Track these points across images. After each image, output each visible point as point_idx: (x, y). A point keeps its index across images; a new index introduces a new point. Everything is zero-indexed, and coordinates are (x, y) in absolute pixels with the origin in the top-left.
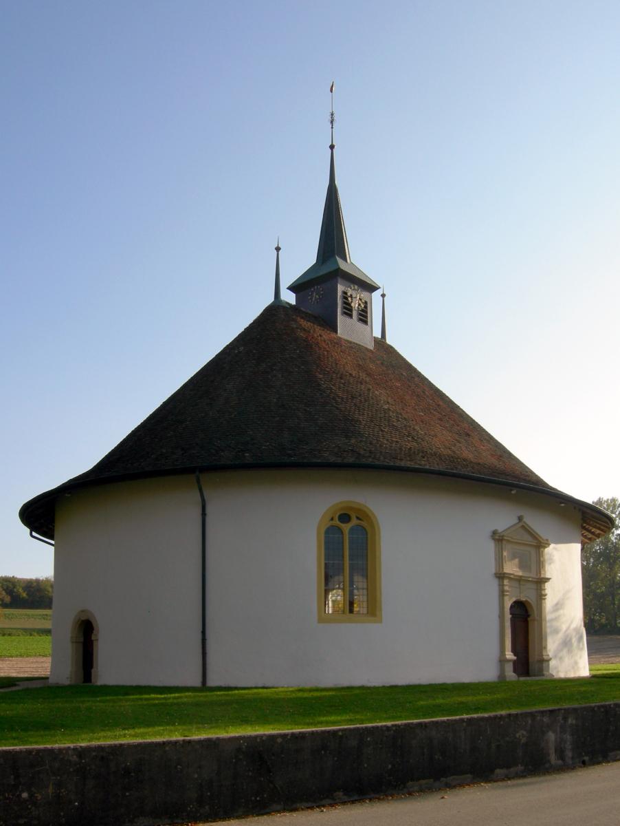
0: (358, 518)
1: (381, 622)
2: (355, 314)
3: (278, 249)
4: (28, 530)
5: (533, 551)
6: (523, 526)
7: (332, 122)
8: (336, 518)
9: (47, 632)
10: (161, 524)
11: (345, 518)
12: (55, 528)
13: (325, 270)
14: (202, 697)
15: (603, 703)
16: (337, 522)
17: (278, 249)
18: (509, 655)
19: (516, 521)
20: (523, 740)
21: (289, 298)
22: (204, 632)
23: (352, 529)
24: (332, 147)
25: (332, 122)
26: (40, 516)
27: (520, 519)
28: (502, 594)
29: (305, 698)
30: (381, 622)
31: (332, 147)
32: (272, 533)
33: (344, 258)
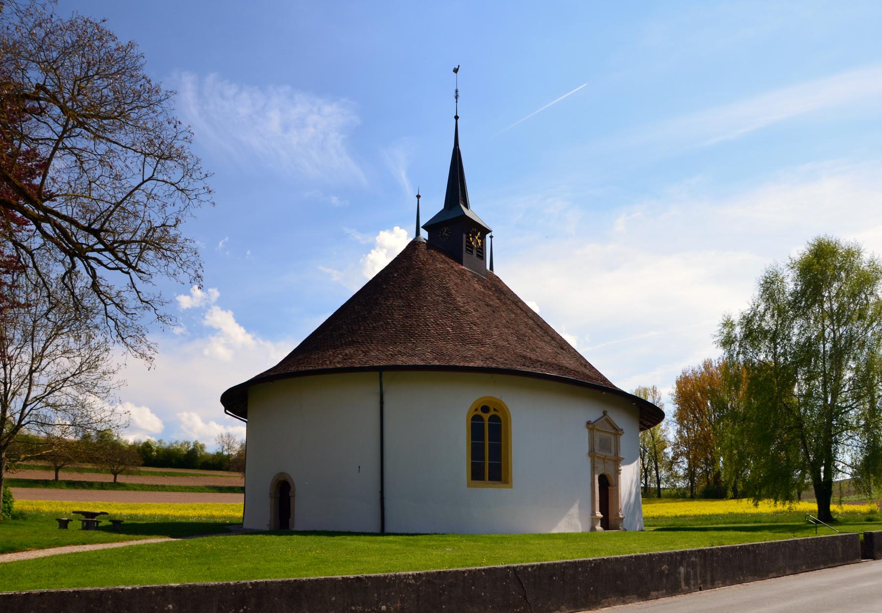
0: (495, 410)
1: (468, 486)
2: (475, 252)
3: (418, 197)
4: (223, 408)
5: (612, 437)
6: (606, 419)
7: (456, 98)
8: (480, 409)
9: (242, 490)
10: (344, 413)
11: (485, 409)
12: (249, 407)
13: (452, 215)
14: (825, 532)
15: (80, 589)
16: (480, 413)
17: (418, 197)
18: (599, 515)
19: (602, 414)
20: (666, 572)
21: (424, 234)
22: (382, 492)
23: (490, 419)
24: (457, 117)
25: (456, 98)
26: (236, 400)
27: (605, 413)
28: (593, 469)
29: (77, 553)
30: (468, 486)
31: (457, 117)
32: (434, 423)
33: (467, 206)
